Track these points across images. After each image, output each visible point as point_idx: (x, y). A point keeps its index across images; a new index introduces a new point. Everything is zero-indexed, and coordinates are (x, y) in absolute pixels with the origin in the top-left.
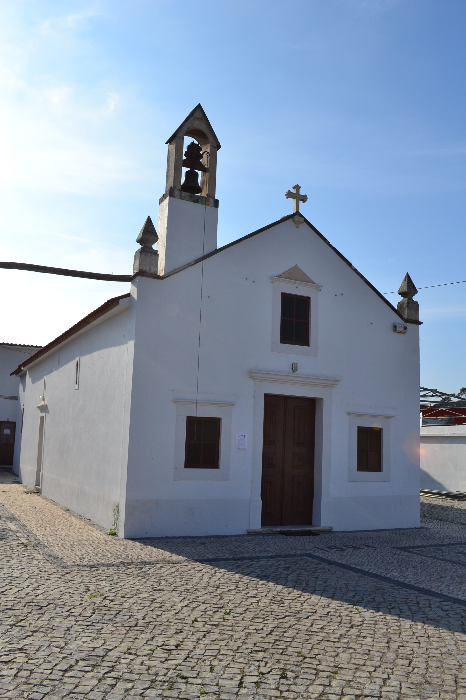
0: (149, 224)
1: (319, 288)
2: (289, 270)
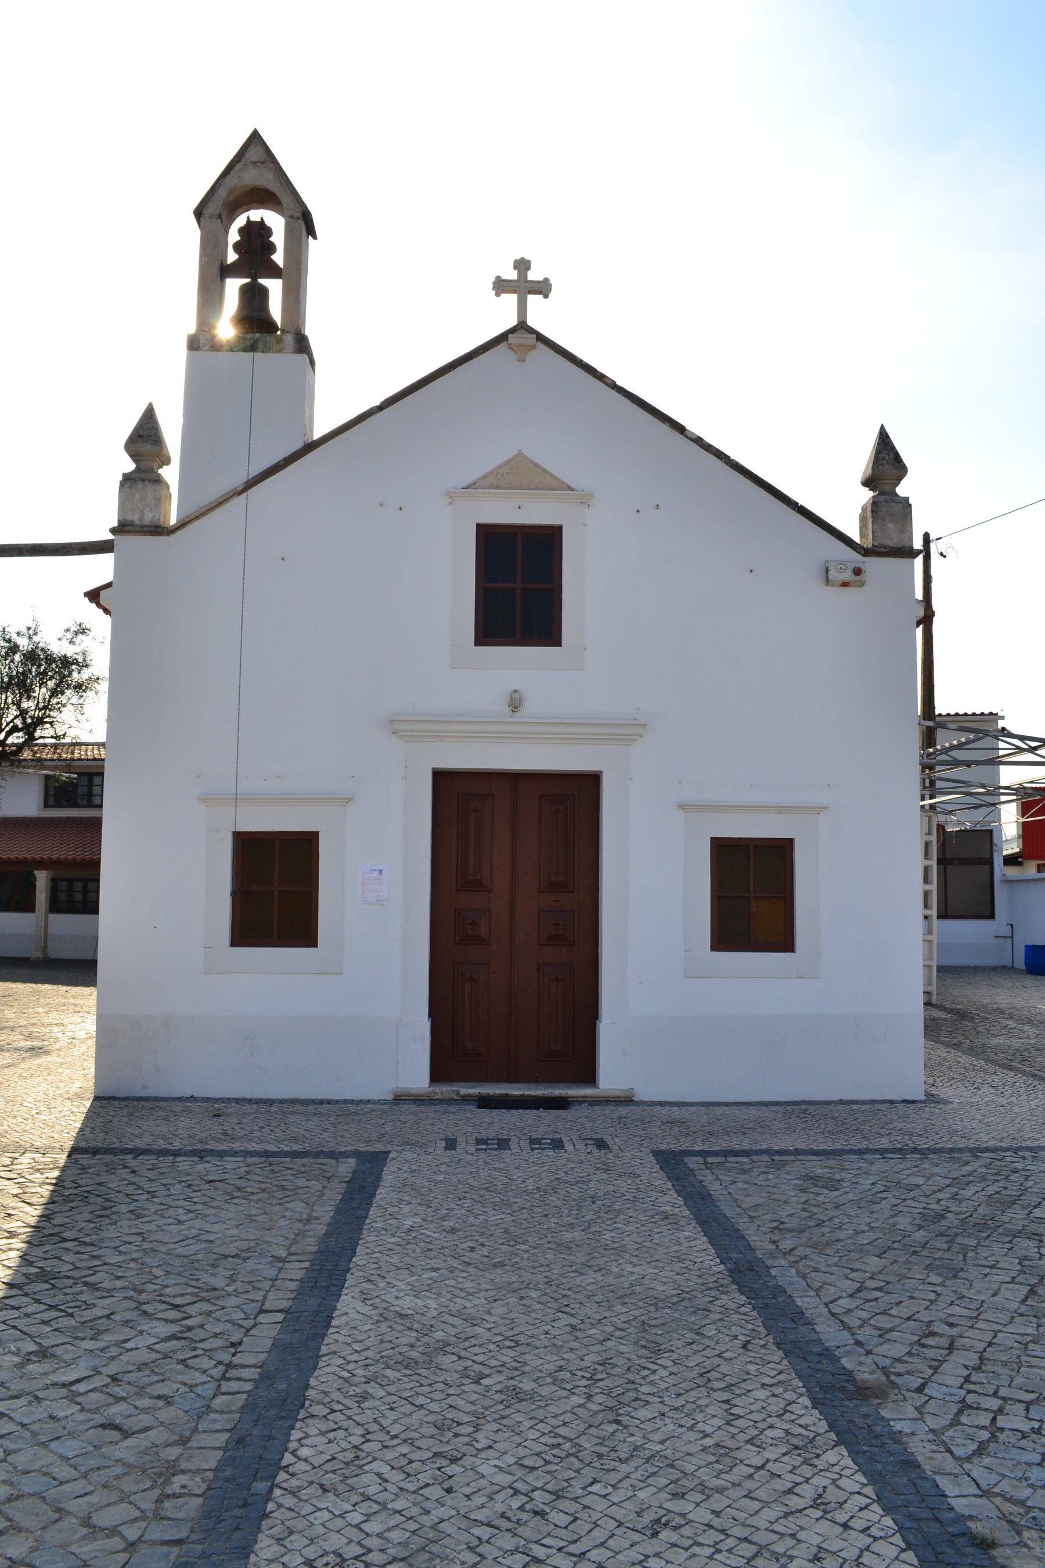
0: (149, 418)
1: (585, 499)
2: (500, 467)
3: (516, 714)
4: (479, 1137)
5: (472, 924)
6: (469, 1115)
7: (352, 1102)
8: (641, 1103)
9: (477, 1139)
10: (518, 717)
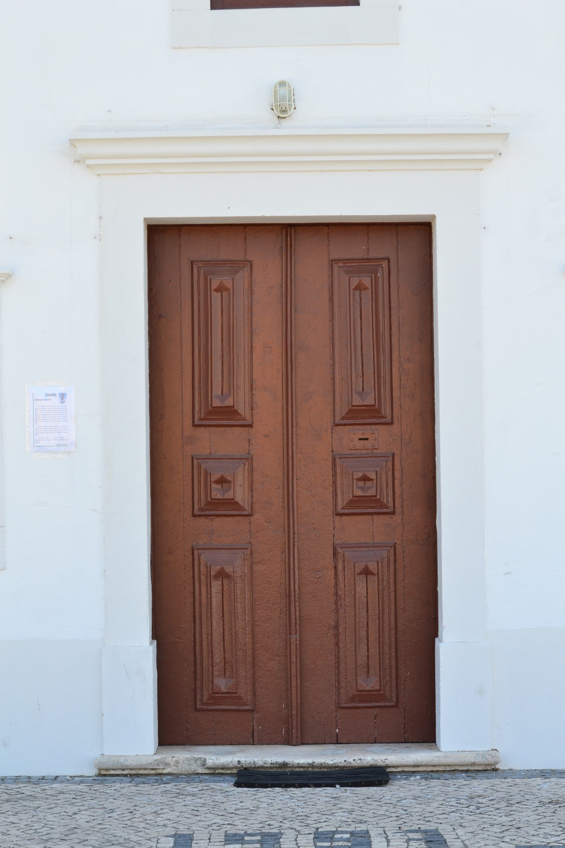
3: (284, 123)
4: (232, 831)
5: (222, 481)
6: (219, 797)
7: (29, 780)
8: (511, 773)
9: (227, 835)
10: (286, 128)
